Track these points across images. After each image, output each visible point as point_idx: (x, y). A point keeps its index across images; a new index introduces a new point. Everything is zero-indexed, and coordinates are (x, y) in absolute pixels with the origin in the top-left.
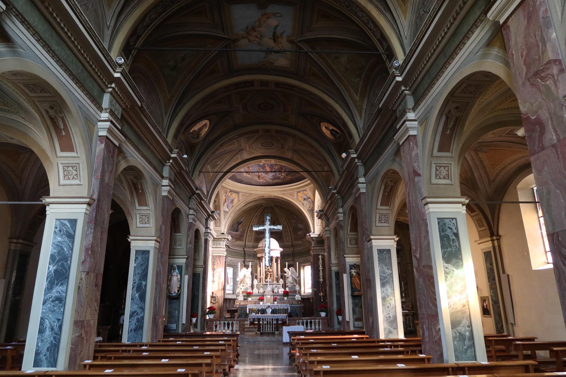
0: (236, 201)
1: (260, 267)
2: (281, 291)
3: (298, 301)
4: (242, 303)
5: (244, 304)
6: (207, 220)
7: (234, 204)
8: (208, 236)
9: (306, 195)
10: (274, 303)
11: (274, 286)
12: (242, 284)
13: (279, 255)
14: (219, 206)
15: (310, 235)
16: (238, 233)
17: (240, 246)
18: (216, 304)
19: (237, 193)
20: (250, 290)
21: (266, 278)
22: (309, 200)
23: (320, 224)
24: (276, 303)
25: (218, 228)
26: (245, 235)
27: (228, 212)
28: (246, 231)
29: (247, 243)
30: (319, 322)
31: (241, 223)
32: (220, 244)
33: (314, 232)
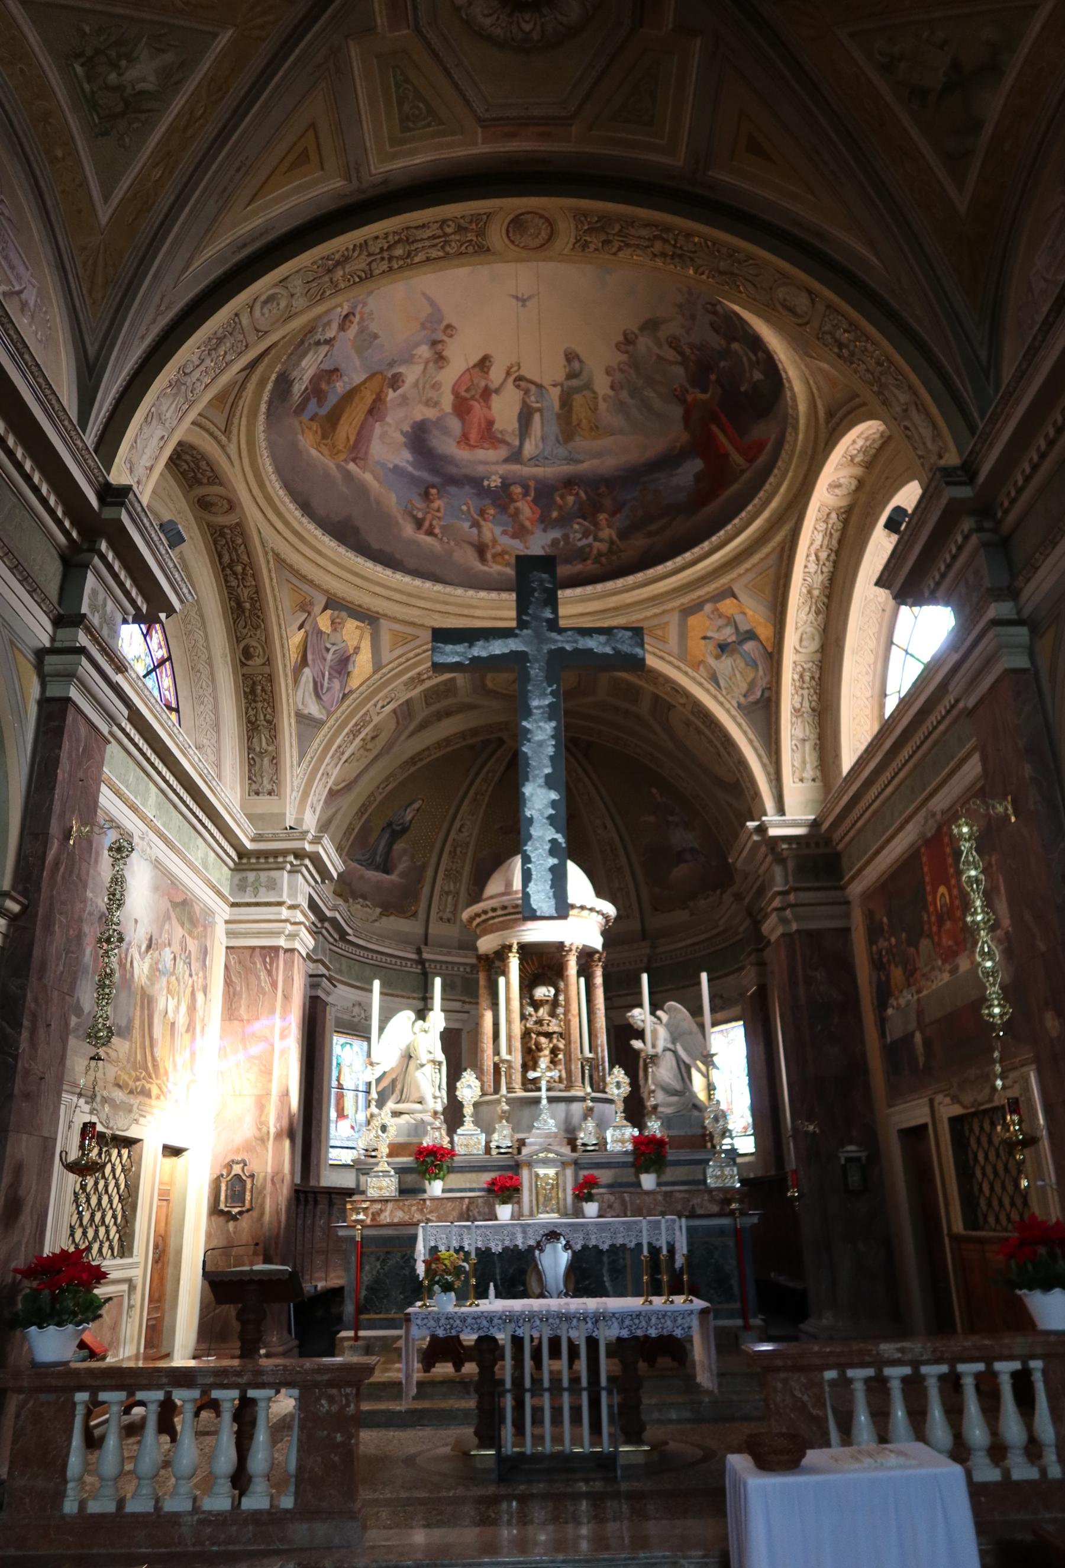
0: (362, 664)
1: (495, 1006)
2: (620, 1137)
3: (726, 1196)
4: (390, 1215)
5: (399, 1216)
6: (74, 565)
7: (354, 682)
8: (70, 675)
9: (731, 621)
10: (578, 1213)
11: (577, 1108)
12: (391, 1105)
13: (597, 942)
14: (271, 678)
15: (762, 829)
16: (393, 877)
17: (403, 940)
18: (245, 1222)
19: (369, 618)
20: (435, 1136)
21: (530, 1060)
22: (749, 646)
23: (809, 773)
24: (591, 1209)
25: (264, 804)
26: (426, 891)
27: (320, 724)
28: (430, 872)
29: (436, 929)
30: (1022, 1382)
31: (404, 830)
32: (272, 886)
33: (781, 811)
